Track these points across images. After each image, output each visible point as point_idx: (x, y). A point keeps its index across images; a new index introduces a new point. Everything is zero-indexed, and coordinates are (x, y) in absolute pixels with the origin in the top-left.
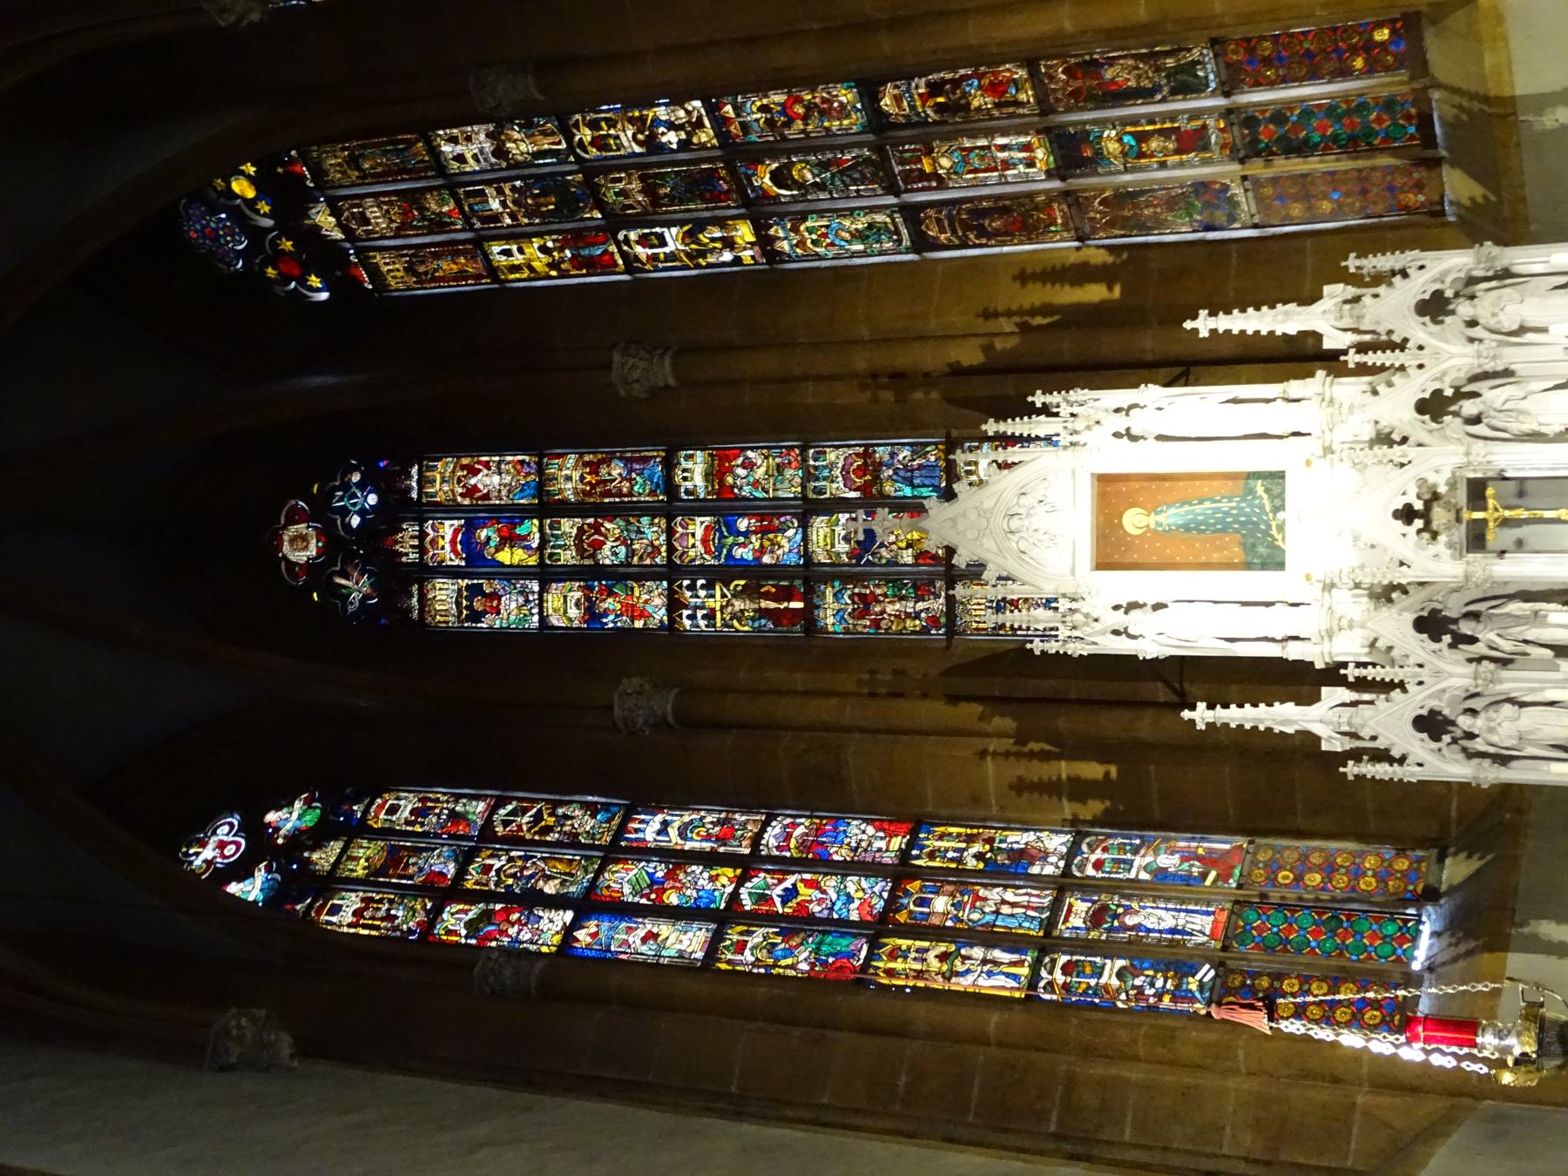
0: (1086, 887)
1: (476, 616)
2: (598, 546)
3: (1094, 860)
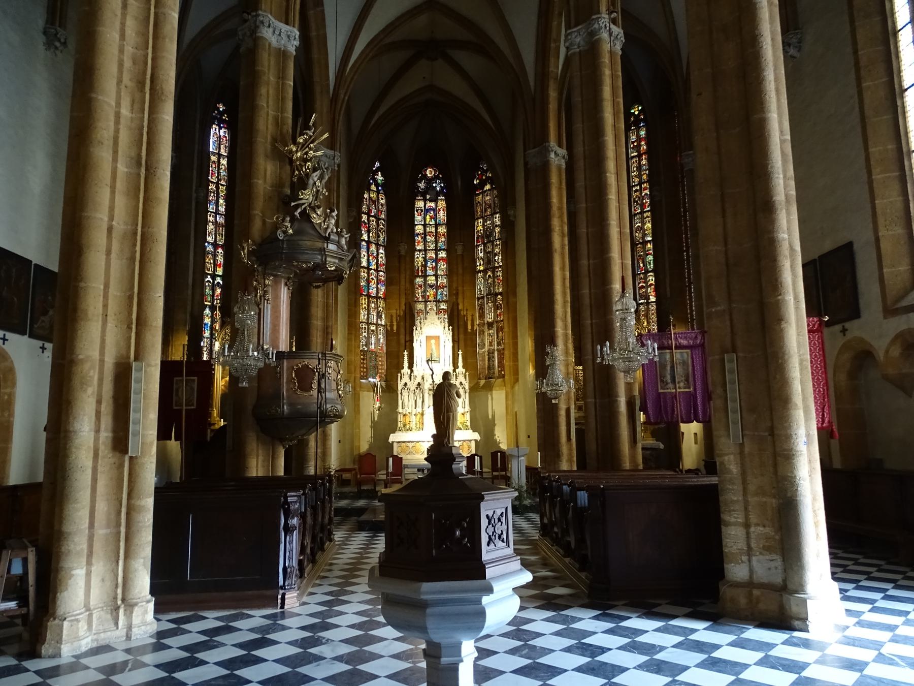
0: (377, 328)
1: (417, 211)
2: (430, 236)
3: (381, 329)
